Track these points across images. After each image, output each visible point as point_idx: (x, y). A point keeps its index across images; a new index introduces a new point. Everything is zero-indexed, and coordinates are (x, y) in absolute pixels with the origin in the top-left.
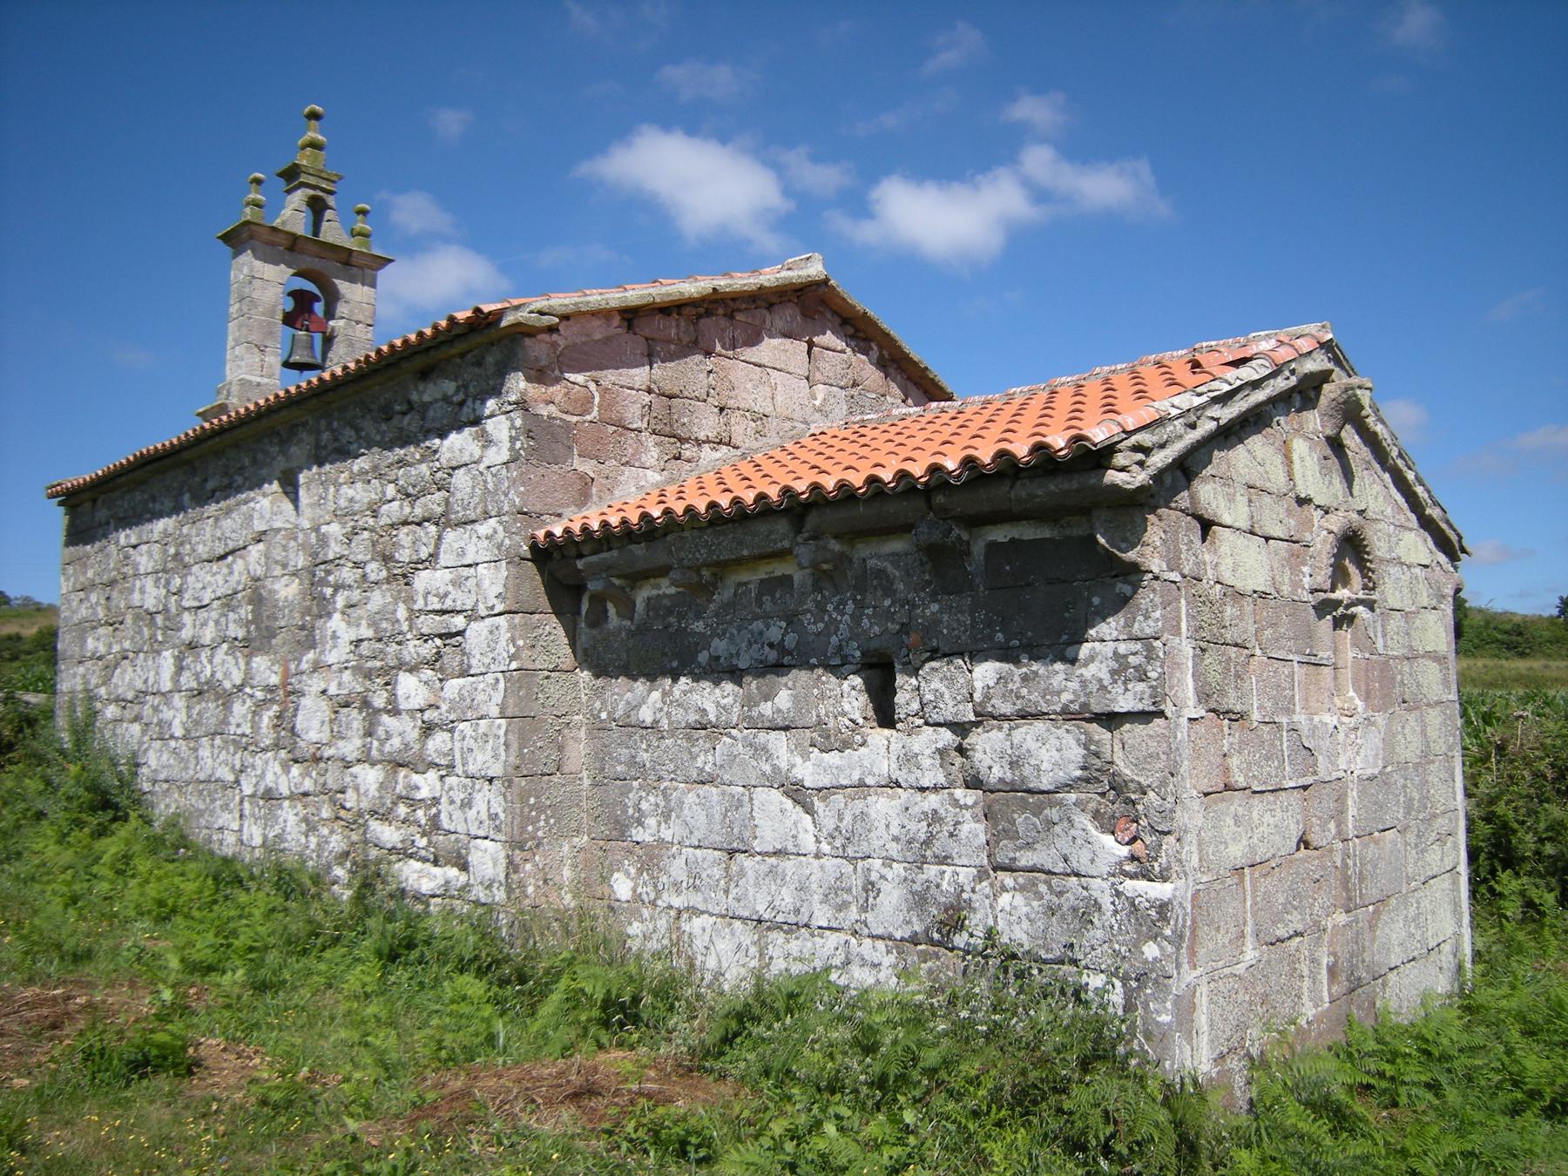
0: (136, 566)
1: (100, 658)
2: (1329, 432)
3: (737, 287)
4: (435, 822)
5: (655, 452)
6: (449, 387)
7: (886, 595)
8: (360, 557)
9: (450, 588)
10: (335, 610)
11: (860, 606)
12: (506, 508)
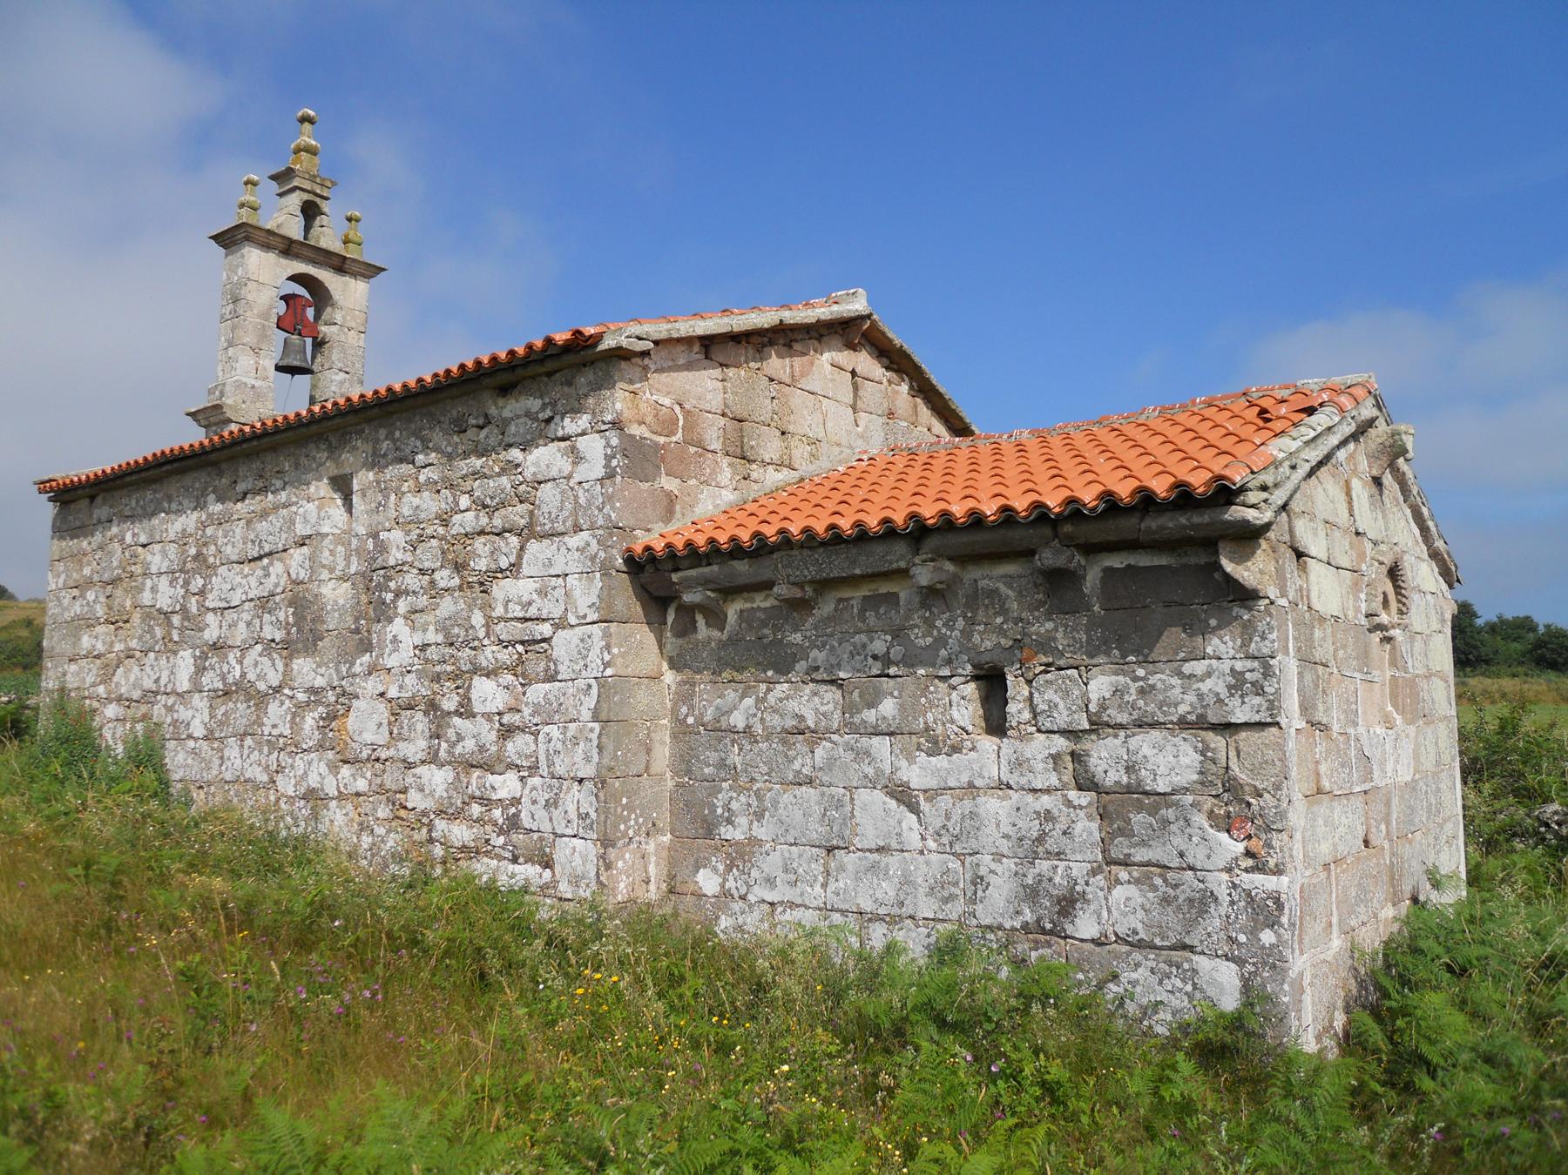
0: (146, 565)
1: (97, 657)
2: (1375, 472)
3: (798, 320)
4: (513, 823)
5: (728, 472)
6: (534, 404)
7: (997, 614)
8: (427, 565)
9: (535, 596)
10: (396, 615)
11: (972, 622)
12: (600, 522)
